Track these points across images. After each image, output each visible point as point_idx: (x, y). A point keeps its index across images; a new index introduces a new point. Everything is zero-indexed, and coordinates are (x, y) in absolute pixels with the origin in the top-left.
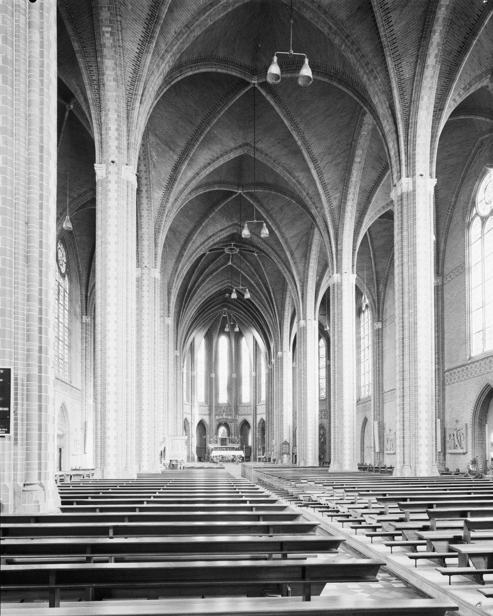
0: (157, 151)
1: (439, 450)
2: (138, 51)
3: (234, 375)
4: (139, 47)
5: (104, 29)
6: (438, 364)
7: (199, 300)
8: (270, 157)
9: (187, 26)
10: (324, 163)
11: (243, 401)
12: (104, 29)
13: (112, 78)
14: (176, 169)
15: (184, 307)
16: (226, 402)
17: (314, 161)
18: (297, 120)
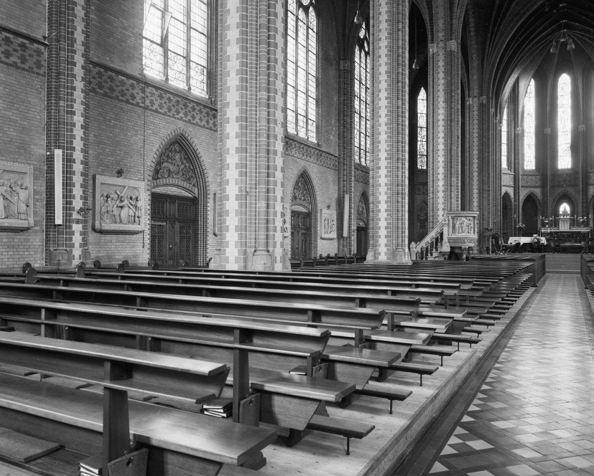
7: (515, 20)
15: (491, 40)
16: (570, 167)
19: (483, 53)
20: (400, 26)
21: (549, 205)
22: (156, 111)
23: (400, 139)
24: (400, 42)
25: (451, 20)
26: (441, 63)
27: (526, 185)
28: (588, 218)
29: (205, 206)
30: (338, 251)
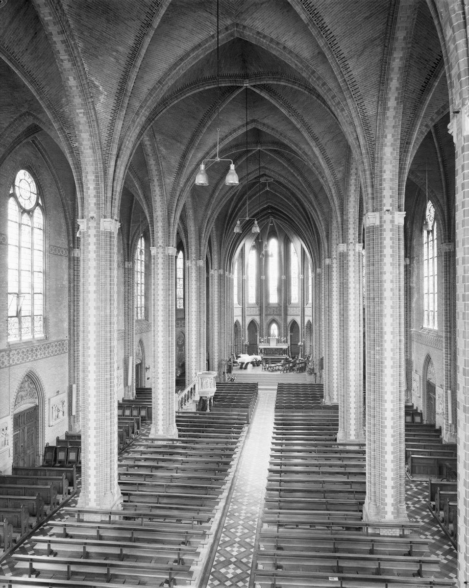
0: (165, 146)
1: (450, 422)
2: (111, 118)
3: (283, 277)
4: (112, 115)
5: (78, 111)
6: (450, 332)
8: (277, 131)
9: (159, 82)
10: (325, 140)
11: (292, 302)
12: (78, 111)
13: (88, 147)
14: (184, 157)
15: (226, 229)
17: (316, 139)
18: (295, 106)
19: (221, 242)
20: (170, 293)
21: (264, 327)
22: (16, 364)
23: (171, 360)
24: (171, 302)
25: (200, 246)
26: (194, 275)
27: (249, 314)
28: (287, 339)
29: (43, 410)
30: (125, 395)
